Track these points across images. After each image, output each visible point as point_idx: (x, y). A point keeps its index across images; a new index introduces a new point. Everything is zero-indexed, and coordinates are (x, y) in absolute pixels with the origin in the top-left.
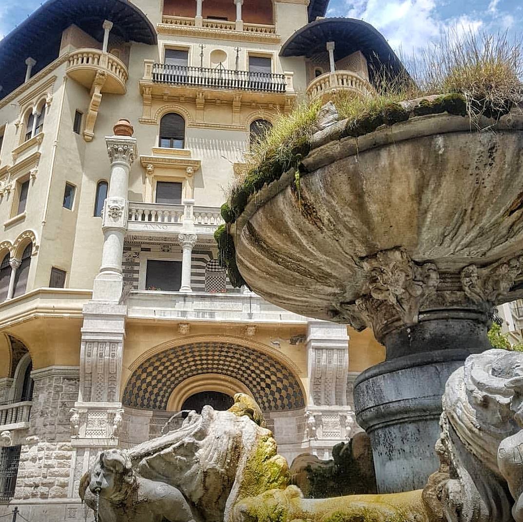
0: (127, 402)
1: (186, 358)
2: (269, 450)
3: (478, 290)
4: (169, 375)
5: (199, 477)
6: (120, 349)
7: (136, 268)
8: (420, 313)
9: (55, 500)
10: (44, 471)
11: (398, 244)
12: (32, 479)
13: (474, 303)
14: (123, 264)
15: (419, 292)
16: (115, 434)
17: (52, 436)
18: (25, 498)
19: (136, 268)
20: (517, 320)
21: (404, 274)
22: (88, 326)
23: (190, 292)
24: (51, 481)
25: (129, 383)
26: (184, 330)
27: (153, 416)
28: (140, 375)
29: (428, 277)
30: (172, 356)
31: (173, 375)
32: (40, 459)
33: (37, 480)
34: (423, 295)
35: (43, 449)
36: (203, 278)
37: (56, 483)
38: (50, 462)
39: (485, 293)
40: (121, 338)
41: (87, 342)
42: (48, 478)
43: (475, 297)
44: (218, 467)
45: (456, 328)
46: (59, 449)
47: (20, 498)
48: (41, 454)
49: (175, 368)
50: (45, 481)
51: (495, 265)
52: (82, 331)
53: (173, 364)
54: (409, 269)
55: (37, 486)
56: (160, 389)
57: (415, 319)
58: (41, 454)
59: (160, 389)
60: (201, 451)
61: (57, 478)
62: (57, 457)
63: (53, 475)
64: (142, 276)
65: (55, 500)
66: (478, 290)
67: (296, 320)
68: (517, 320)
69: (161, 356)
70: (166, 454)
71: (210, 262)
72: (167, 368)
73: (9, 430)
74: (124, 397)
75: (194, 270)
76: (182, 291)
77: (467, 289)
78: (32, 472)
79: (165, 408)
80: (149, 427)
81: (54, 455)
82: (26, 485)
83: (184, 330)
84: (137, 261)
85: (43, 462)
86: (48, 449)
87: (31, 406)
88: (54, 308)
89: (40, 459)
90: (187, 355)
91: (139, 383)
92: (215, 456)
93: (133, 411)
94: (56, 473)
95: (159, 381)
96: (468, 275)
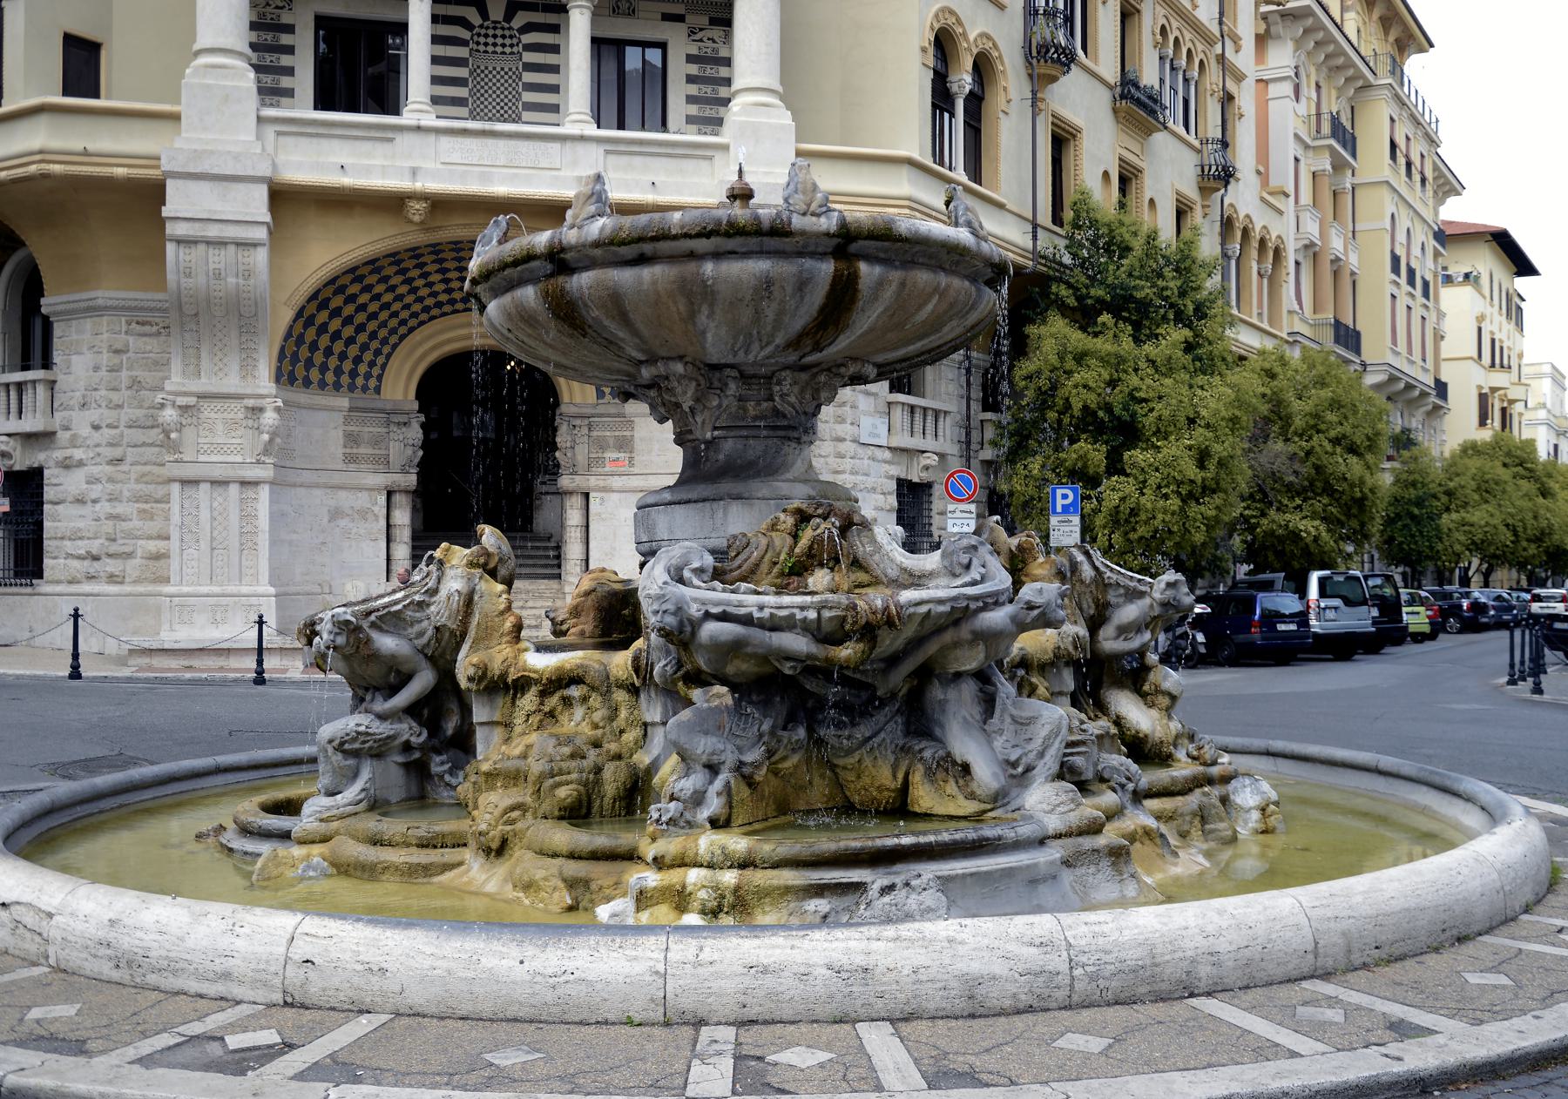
0: (286, 375)
1: (425, 275)
2: (502, 607)
3: (792, 399)
4: (384, 315)
5: (430, 632)
6: (261, 256)
7: (285, 39)
8: (715, 428)
9: (140, 589)
10: (108, 527)
11: (681, 353)
12: (80, 543)
13: (784, 416)
14: (254, 26)
15: (715, 403)
16: (266, 451)
17: (118, 452)
18: (70, 582)
19: (285, 39)
20: (1307, 147)
21: (694, 384)
22: (179, 201)
23: (430, 120)
24: (127, 549)
25: (288, 335)
26: (417, 209)
27: (351, 409)
28: (313, 317)
29: (726, 385)
30: (389, 271)
31: (395, 315)
32: (95, 501)
33: (95, 546)
34: (720, 406)
35: (98, 480)
36: (462, 72)
37: (139, 553)
38: (120, 509)
39: (801, 403)
40: (261, 234)
41: (179, 241)
42: (121, 542)
43: (788, 410)
44: (449, 624)
45: (755, 448)
46: (137, 481)
47: (58, 582)
48: (96, 491)
49: (400, 298)
50: (113, 548)
51: (815, 370)
52: (164, 214)
53: (392, 289)
54: (700, 378)
55: (96, 558)
56: (364, 347)
57: (708, 435)
58: (96, 491)
59: (364, 347)
60: (433, 608)
61: (141, 542)
62: (138, 499)
63: (130, 535)
64: (304, 80)
65: (140, 589)
66: (792, 399)
67: (691, 195)
68: (1307, 147)
69: (364, 271)
70: (396, 612)
71: (481, 26)
72: (377, 297)
73: (9, 435)
74: (279, 369)
75: (442, 50)
76: (407, 117)
77: (777, 398)
78: (80, 530)
79: (378, 390)
80: (341, 434)
81: (126, 494)
82: (69, 556)
83: (417, 209)
84: (286, 18)
85: (104, 508)
86: (111, 480)
87: (54, 382)
88: (86, 153)
89: (95, 501)
90: (427, 269)
91: (311, 334)
92: (446, 614)
93: (303, 397)
94: (136, 532)
95: (361, 328)
96: (779, 383)
